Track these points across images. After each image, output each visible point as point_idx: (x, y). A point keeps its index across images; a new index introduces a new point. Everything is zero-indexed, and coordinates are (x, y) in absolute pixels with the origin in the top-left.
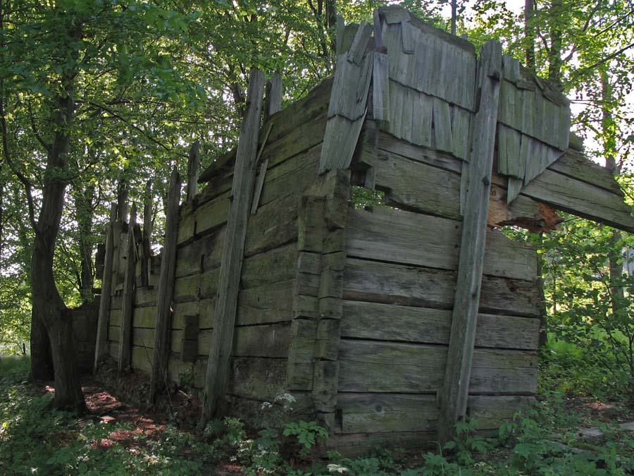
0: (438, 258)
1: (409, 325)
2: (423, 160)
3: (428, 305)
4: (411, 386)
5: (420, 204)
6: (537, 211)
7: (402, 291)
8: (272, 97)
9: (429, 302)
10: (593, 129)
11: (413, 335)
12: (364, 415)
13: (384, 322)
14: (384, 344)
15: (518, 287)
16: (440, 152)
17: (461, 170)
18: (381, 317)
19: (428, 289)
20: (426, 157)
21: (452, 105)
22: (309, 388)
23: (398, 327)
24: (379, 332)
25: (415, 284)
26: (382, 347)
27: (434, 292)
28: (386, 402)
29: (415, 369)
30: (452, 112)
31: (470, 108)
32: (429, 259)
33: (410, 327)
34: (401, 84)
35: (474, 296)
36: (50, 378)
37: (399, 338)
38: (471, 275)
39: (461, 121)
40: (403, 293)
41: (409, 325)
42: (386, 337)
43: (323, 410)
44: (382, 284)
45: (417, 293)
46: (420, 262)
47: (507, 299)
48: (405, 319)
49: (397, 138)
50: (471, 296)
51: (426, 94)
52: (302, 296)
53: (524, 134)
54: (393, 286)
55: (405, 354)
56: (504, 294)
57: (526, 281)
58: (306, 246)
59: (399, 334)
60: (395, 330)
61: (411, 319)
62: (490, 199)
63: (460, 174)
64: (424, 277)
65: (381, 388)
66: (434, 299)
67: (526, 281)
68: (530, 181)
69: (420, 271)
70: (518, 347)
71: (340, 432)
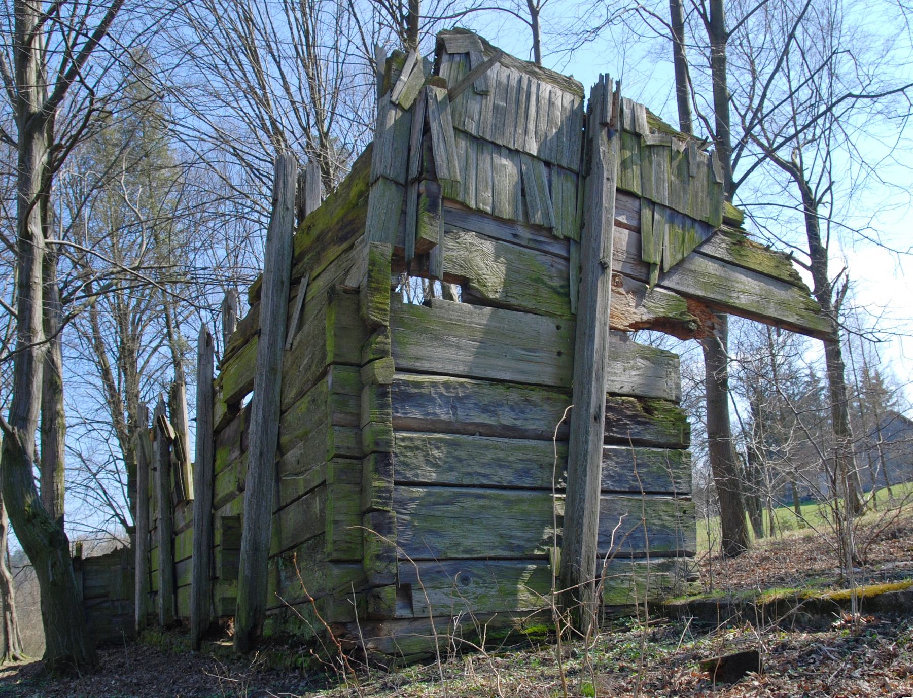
0: (546, 373)
1: (499, 463)
2: (510, 238)
3: (521, 434)
4: (510, 547)
5: (510, 299)
6: (684, 309)
7: (485, 416)
8: (571, 208)
9: (526, 430)
10: (154, 25)
11: (505, 476)
12: (446, 590)
13: (460, 460)
14: (464, 490)
15: (656, 409)
16: (538, 228)
17: (569, 252)
18: (456, 453)
19: (523, 412)
20: (515, 236)
21: (548, 164)
22: (358, 557)
23: (484, 465)
24: (453, 473)
25: (502, 405)
26: (465, 495)
27: (531, 417)
28: (476, 572)
29: (512, 522)
30: (550, 175)
31: (575, 167)
32: (523, 372)
33: (500, 466)
34: (471, 135)
35: (597, 418)
36: (566, 469)
37: (485, 482)
38: (590, 392)
39: (565, 187)
40: (485, 419)
41: (499, 463)
42: (466, 481)
43: (377, 582)
44: (454, 408)
45: (507, 418)
46: (508, 376)
47: (639, 423)
48: (490, 455)
49: (471, 209)
50: (592, 419)
51: (510, 150)
52: (337, 428)
53: (658, 204)
54: (469, 409)
55: (495, 503)
56: (635, 416)
57: (666, 400)
58: (336, 355)
59: (485, 476)
60: (479, 470)
61: (501, 455)
62: (612, 290)
63: (567, 259)
64: (515, 396)
65: (465, 552)
66: (531, 427)
67: (666, 400)
68: (671, 268)
69: (508, 388)
70: (663, 490)
71: (411, 616)
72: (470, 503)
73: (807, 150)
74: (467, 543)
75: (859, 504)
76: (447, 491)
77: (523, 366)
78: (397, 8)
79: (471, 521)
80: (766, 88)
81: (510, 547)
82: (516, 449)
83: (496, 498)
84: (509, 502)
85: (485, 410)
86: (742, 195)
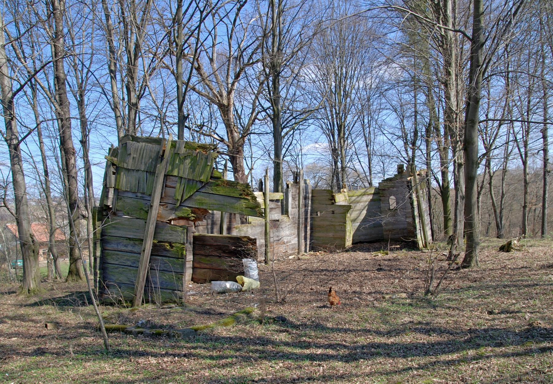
4: (130, 281)
11: (129, 263)
41: (128, 260)
48: (125, 258)
61: (128, 258)
64: (132, 242)
72: (121, 269)
73: (227, 176)
74: (120, 279)
75: (314, 360)
76: (117, 266)
77: (135, 234)
78: (488, 32)
79: (121, 274)
80: (228, 75)
81: (130, 281)
82: (132, 256)
83: (127, 268)
84: (130, 270)
85: (125, 246)
86: (281, 94)
